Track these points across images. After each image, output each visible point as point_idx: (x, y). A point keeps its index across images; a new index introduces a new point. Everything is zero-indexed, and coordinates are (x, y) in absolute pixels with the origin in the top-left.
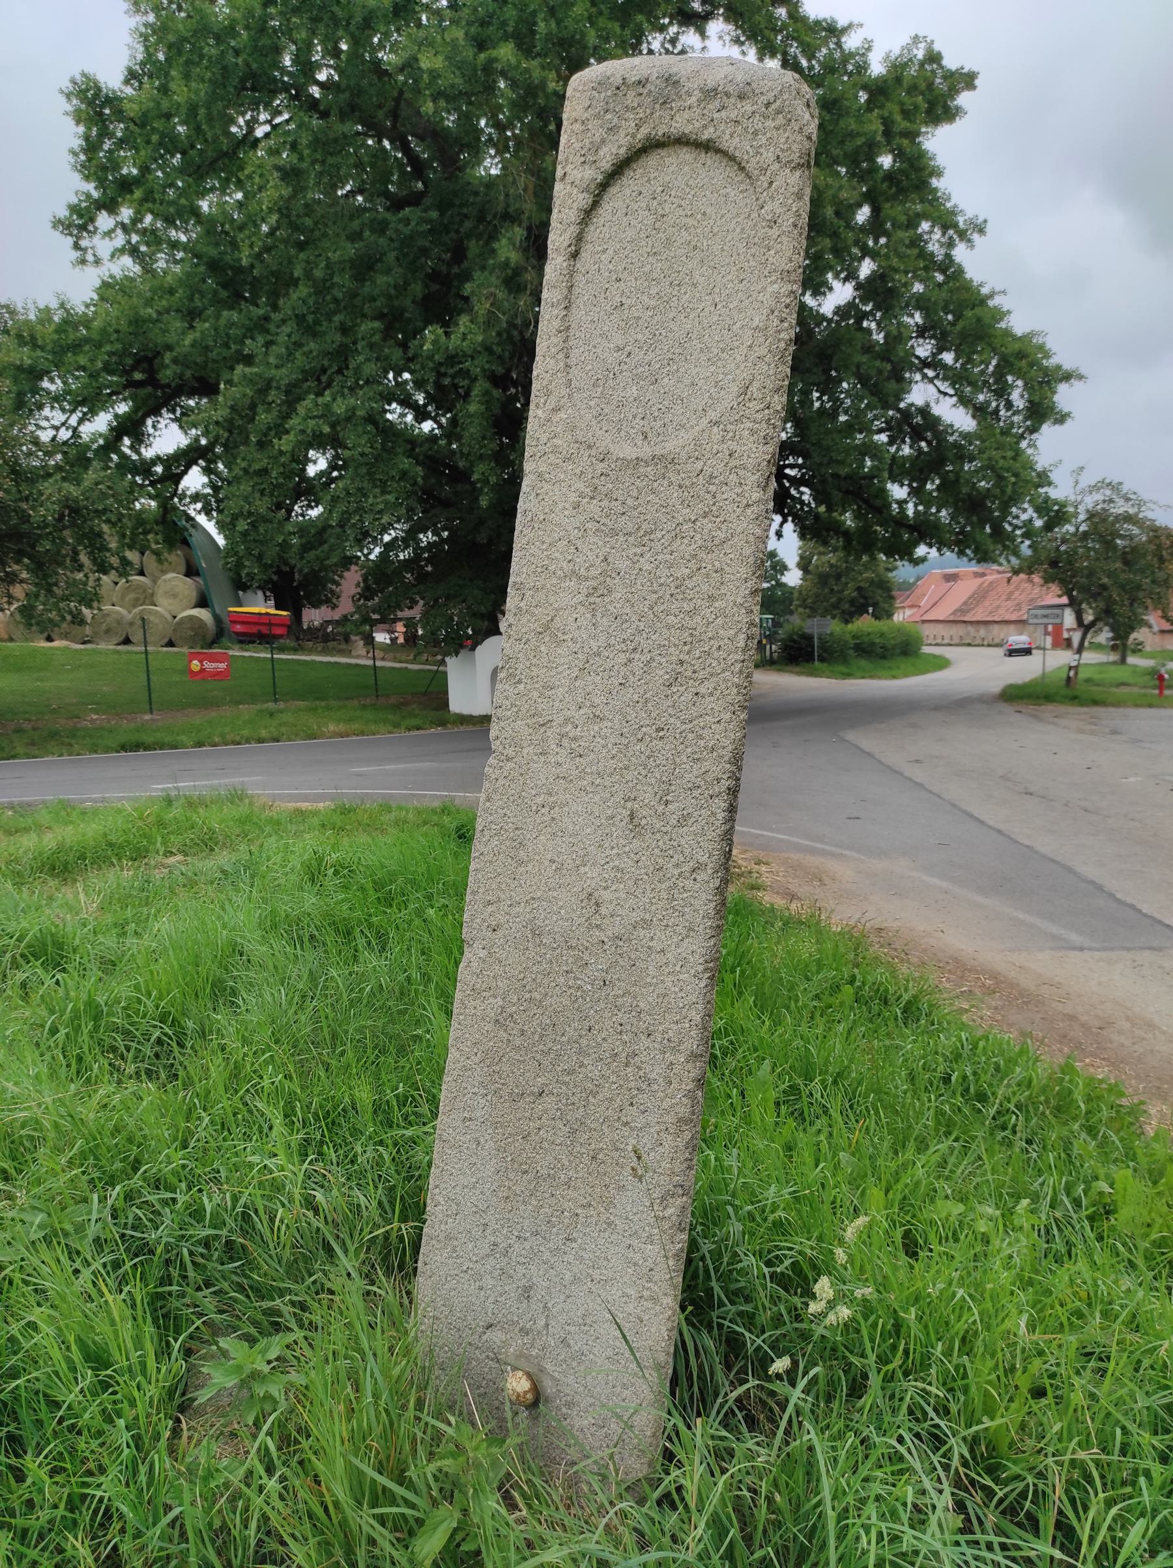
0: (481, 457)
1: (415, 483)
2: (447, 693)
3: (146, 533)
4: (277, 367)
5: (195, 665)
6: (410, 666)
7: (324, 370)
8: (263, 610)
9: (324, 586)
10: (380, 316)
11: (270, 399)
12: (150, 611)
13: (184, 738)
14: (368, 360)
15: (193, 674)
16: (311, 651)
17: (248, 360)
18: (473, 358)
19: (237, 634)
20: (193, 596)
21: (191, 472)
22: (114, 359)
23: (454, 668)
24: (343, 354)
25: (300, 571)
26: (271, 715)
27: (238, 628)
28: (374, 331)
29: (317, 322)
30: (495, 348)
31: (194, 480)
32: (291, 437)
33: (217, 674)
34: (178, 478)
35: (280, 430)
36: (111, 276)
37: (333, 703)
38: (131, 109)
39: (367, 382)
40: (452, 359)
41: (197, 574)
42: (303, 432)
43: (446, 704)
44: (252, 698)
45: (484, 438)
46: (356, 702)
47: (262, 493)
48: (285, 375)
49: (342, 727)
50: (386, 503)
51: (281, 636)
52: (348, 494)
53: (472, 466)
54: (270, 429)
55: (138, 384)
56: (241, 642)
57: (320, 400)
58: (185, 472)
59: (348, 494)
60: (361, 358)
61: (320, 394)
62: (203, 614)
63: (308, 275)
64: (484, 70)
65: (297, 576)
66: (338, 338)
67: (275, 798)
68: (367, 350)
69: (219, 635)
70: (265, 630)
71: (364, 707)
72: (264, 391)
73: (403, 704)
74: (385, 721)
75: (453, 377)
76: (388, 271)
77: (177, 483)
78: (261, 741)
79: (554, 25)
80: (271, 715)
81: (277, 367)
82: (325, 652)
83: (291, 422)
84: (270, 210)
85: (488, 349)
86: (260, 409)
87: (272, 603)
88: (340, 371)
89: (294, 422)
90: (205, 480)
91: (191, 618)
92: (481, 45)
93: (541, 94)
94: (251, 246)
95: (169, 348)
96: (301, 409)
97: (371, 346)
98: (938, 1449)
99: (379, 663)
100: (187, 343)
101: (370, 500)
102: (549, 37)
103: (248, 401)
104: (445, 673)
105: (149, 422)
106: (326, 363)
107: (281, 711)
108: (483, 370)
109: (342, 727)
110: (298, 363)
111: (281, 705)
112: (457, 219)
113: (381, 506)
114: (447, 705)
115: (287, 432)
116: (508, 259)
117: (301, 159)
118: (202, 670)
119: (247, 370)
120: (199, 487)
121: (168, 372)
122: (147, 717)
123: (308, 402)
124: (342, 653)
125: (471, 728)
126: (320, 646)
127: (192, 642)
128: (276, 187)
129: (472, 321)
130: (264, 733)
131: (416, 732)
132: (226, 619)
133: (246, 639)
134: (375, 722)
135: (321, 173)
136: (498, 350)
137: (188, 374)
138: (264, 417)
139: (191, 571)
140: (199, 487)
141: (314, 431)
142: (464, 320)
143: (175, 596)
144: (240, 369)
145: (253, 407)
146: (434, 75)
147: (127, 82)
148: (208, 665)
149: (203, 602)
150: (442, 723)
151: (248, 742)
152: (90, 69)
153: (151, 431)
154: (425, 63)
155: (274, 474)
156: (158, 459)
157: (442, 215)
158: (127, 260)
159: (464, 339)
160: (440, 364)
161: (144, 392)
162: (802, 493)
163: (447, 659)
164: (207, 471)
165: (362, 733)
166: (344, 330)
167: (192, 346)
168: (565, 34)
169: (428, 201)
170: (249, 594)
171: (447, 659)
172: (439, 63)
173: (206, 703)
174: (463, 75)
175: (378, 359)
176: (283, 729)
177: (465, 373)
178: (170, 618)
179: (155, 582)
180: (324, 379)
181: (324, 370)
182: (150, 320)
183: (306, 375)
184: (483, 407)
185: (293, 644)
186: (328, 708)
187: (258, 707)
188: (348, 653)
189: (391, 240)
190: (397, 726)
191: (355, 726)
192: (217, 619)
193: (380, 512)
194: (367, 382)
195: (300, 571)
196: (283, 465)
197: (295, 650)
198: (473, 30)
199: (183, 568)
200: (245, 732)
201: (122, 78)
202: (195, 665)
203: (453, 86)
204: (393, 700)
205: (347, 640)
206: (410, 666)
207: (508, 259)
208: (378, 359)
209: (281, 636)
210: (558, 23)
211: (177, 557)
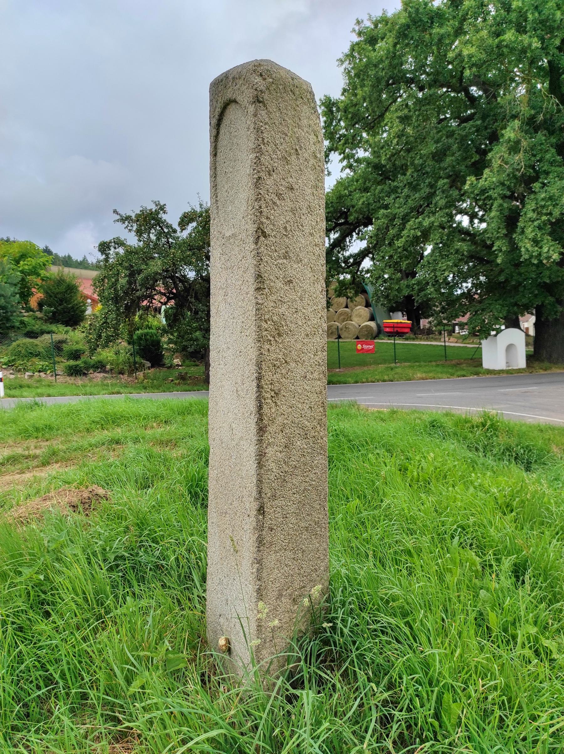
0: (498, 238)
1: (463, 255)
2: (481, 358)
3: (346, 289)
4: (399, 208)
5: (359, 347)
6: (468, 346)
7: (421, 206)
8: (399, 321)
9: (431, 309)
10: (449, 177)
11: (395, 223)
12: (349, 324)
13: (350, 379)
14: (441, 198)
15: (358, 351)
16: (421, 339)
17: (386, 207)
18: (494, 189)
19: (387, 332)
20: (368, 316)
21: (365, 260)
22: (330, 215)
23: (485, 344)
24: (429, 197)
25: (417, 301)
26: (392, 369)
27: (388, 330)
28: (445, 184)
29: (418, 185)
30: (506, 182)
31: (367, 263)
32: (403, 239)
33: (368, 351)
34: (359, 264)
35: (398, 236)
36: (341, 178)
37: (422, 363)
38: (341, 106)
39: (441, 209)
40: (483, 191)
41: (370, 306)
42: (408, 236)
43: (481, 365)
44: (384, 361)
45: (499, 228)
46: (434, 363)
47: (390, 267)
48: (402, 211)
49: (424, 375)
50: (448, 266)
51: (407, 333)
52: (429, 263)
53: (493, 243)
54: (394, 237)
55: (341, 224)
56: (389, 336)
57: (417, 220)
58: (362, 260)
59: (429, 263)
60: (438, 198)
61: (417, 218)
62: (372, 324)
63: (412, 163)
64: (497, 47)
65: (415, 304)
66: (428, 190)
67: (368, 406)
68: (441, 193)
69: (379, 333)
70: (399, 330)
71: (437, 366)
72: (393, 219)
73: (458, 364)
74: (447, 372)
75: (484, 200)
76: (453, 155)
77: (359, 266)
78: (384, 381)
79: (537, 14)
80: (392, 369)
81: (399, 208)
82: (427, 339)
83: (403, 232)
84: (394, 137)
85: (503, 184)
86: (390, 228)
87: (406, 318)
88: (428, 206)
89: (405, 232)
90: (372, 263)
91: (367, 326)
92: (498, 34)
93: (529, 51)
94: (386, 155)
95: (353, 207)
96: (408, 226)
97: (443, 192)
98: (396, 707)
99: (447, 344)
100: (360, 203)
101: (440, 265)
102: (534, 21)
103: (385, 226)
104: (481, 348)
105: (348, 240)
106: (422, 203)
107: (396, 368)
108: (499, 195)
109: (424, 375)
110: (409, 205)
111: (398, 365)
112: (492, 122)
113: (445, 268)
114: (482, 365)
115: (402, 237)
116: (509, 137)
117: (410, 111)
118: (362, 349)
119: (385, 211)
120: (369, 267)
121: (352, 217)
122: (338, 370)
123: (411, 223)
124: (436, 340)
125: (493, 376)
126: (425, 337)
127: (367, 336)
128: (397, 126)
129: (491, 171)
130: (386, 378)
131: (462, 378)
132: (382, 325)
133: (391, 335)
134: (441, 373)
135: (419, 116)
136: (507, 183)
137: (361, 216)
138: (392, 232)
139: (368, 305)
140: (369, 267)
141: (413, 236)
142: (487, 171)
143: (360, 316)
144: (382, 211)
145: (387, 228)
146: (470, 56)
147: (343, 94)
148: (365, 347)
149: (372, 318)
150: (477, 374)
151: (378, 381)
152: (327, 94)
153: (348, 244)
154: (465, 52)
155: (395, 257)
156: (351, 256)
157: (484, 122)
158: (348, 171)
159: (486, 181)
160: (477, 195)
161: (344, 227)
162: (536, 242)
163: (482, 341)
164: (373, 259)
165: (434, 378)
166: (431, 186)
167: (363, 204)
168: (543, 17)
169: (476, 117)
170: (395, 313)
171: (482, 341)
172: (473, 50)
173: (363, 364)
174: (486, 53)
175: (446, 197)
176: (396, 376)
177: (490, 198)
178: (357, 326)
179: (352, 310)
180: (420, 210)
181: (421, 206)
182: (346, 195)
183: (412, 209)
184: (498, 213)
185: (412, 336)
186: (420, 366)
187: (386, 365)
188: (439, 340)
189: (456, 139)
190: (452, 375)
191: (431, 375)
192: (378, 326)
193: (444, 270)
194: (441, 209)
195: (417, 301)
196: (400, 253)
197: (414, 339)
198: (493, 29)
199: (364, 304)
200: (377, 377)
201: (341, 93)
202: (359, 347)
203: (480, 60)
204: (453, 362)
205: (440, 333)
206: (468, 346)
207: (509, 137)
208: (446, 197)
209: (407, 333)
210: (539, 13)
211: (360, 298)
